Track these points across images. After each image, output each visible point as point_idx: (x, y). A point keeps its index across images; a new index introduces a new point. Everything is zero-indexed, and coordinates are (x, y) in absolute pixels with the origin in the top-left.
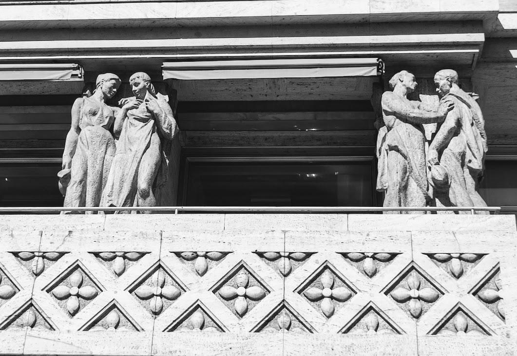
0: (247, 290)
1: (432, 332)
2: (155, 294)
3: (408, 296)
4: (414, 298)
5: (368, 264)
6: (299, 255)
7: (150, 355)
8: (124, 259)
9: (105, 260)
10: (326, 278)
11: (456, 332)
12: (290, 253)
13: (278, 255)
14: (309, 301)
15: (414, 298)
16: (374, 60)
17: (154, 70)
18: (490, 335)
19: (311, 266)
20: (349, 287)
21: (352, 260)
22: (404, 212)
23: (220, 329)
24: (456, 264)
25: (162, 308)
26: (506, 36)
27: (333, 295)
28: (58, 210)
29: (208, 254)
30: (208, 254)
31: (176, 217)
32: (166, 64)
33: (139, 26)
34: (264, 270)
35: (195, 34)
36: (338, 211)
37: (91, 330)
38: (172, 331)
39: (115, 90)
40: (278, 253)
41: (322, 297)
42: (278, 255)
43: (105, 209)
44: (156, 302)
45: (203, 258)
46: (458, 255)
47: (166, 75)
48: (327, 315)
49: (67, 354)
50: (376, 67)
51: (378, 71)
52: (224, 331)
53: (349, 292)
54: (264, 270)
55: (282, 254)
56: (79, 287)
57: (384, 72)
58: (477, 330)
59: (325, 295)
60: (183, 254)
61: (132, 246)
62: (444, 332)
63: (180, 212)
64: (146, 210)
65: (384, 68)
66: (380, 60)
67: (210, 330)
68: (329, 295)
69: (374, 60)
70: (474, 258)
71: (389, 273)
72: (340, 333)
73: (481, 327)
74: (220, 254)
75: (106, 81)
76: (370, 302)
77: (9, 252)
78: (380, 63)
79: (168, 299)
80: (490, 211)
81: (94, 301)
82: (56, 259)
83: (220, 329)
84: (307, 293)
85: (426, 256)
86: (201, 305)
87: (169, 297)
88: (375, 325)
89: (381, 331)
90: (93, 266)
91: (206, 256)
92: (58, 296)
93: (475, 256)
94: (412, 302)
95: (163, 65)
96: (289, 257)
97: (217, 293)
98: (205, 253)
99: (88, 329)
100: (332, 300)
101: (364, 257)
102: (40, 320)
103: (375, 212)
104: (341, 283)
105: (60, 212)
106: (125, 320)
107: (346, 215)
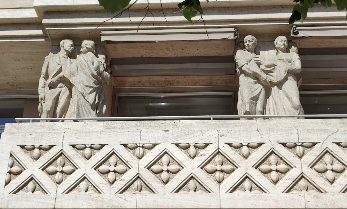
0: (63, 168)
1: (229, 191)
2: (58, 171)
3: (326, 169)
4: (219, 171)
5: (299, 149)
6: (148, 146)
7: (52, 207)
8: (40, 150)
9: (130, 149)
10: (165, 159)
11: (189, 192)
12: (303, 143)
13: (295, 145)
14: (262, 173)
15: (219, 171)
16: (232, 30)
17: (95, 37)
18: (154, 193)
19: (316, 151)
20: (179, 164)
21: (78, 149)
22: (48, 121)
23: (44, 191)
24: (245, 150)
25: (169, 179)
26: (15, 22)
27: (278, 169)
28: (39, 119)
29: (249, 144)
30: (249, 144)
31: (212, 122)
32: (103, 32)
33: (60, 13)
34: (180, 155)
35: (271, 11)
36: (330, 117)
37: (70, 193)
38: (232, 193)
39: (73, 47)
40: (295, 143)
41: (162, 171)
42: (241, 145)
43: (74, 119)
44: (164, 175)
45: (246, 147)
46: (90, 145)
47: (103, 39)
48: (331, 181)
49: (29, 208)
50: (233, 33)
51: (234, 36)
52: (101, 193)
53: (178, 167)
54: (180, 155)
55: (298, 144)
56: (168, 166)
57: (238, 37)
58: (258, 189)
59: (273, 169)
60: (287, 145)
61: (147, 141)
62: (181, 192)
63: (214, 119)
64: (49, 120)
65: (238, 35)
66: (236, 30)
67: (145, 192)
68: (275, 169)
69: (232, 30)
70: (99, 147)
71: (311, 156)
72: (341, 193)
73: (260, 188)
74: (311, 144)
75: (67, 44)
76: (191, 173)
77: (69, 145)
78: (236, 32)
79: (119, 173)
80: (74, 120)
81: (178, 175)
82: (99, 149)
83: (44, 191)
84: (206, 168)
85: (122, 145)
86: (34, 177)
87: (283, 171)
88: (86, 188)
89: (143, 192)
90: (70, 152)
91: (143, 147)
92: (209, 171)
93: (204, 144)
94: (217, 173)
95: (101, 33)
96: (302, 146)
97: (313, 168)
98: (247, 143)
99: (177, 191)
100: (62, 174)
101: (34, 148)
102: (38, 187)
103: (234, 118)
104: (337, 161)
105: (40, 121)
106: (38, 187)
107: (179, 121)
